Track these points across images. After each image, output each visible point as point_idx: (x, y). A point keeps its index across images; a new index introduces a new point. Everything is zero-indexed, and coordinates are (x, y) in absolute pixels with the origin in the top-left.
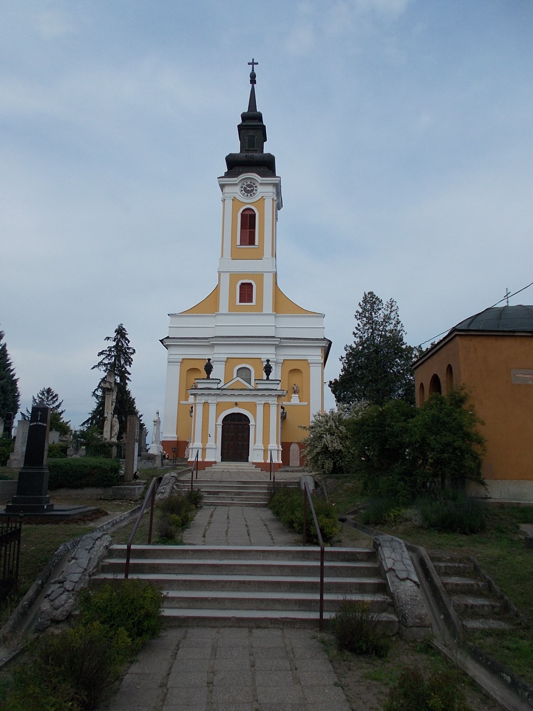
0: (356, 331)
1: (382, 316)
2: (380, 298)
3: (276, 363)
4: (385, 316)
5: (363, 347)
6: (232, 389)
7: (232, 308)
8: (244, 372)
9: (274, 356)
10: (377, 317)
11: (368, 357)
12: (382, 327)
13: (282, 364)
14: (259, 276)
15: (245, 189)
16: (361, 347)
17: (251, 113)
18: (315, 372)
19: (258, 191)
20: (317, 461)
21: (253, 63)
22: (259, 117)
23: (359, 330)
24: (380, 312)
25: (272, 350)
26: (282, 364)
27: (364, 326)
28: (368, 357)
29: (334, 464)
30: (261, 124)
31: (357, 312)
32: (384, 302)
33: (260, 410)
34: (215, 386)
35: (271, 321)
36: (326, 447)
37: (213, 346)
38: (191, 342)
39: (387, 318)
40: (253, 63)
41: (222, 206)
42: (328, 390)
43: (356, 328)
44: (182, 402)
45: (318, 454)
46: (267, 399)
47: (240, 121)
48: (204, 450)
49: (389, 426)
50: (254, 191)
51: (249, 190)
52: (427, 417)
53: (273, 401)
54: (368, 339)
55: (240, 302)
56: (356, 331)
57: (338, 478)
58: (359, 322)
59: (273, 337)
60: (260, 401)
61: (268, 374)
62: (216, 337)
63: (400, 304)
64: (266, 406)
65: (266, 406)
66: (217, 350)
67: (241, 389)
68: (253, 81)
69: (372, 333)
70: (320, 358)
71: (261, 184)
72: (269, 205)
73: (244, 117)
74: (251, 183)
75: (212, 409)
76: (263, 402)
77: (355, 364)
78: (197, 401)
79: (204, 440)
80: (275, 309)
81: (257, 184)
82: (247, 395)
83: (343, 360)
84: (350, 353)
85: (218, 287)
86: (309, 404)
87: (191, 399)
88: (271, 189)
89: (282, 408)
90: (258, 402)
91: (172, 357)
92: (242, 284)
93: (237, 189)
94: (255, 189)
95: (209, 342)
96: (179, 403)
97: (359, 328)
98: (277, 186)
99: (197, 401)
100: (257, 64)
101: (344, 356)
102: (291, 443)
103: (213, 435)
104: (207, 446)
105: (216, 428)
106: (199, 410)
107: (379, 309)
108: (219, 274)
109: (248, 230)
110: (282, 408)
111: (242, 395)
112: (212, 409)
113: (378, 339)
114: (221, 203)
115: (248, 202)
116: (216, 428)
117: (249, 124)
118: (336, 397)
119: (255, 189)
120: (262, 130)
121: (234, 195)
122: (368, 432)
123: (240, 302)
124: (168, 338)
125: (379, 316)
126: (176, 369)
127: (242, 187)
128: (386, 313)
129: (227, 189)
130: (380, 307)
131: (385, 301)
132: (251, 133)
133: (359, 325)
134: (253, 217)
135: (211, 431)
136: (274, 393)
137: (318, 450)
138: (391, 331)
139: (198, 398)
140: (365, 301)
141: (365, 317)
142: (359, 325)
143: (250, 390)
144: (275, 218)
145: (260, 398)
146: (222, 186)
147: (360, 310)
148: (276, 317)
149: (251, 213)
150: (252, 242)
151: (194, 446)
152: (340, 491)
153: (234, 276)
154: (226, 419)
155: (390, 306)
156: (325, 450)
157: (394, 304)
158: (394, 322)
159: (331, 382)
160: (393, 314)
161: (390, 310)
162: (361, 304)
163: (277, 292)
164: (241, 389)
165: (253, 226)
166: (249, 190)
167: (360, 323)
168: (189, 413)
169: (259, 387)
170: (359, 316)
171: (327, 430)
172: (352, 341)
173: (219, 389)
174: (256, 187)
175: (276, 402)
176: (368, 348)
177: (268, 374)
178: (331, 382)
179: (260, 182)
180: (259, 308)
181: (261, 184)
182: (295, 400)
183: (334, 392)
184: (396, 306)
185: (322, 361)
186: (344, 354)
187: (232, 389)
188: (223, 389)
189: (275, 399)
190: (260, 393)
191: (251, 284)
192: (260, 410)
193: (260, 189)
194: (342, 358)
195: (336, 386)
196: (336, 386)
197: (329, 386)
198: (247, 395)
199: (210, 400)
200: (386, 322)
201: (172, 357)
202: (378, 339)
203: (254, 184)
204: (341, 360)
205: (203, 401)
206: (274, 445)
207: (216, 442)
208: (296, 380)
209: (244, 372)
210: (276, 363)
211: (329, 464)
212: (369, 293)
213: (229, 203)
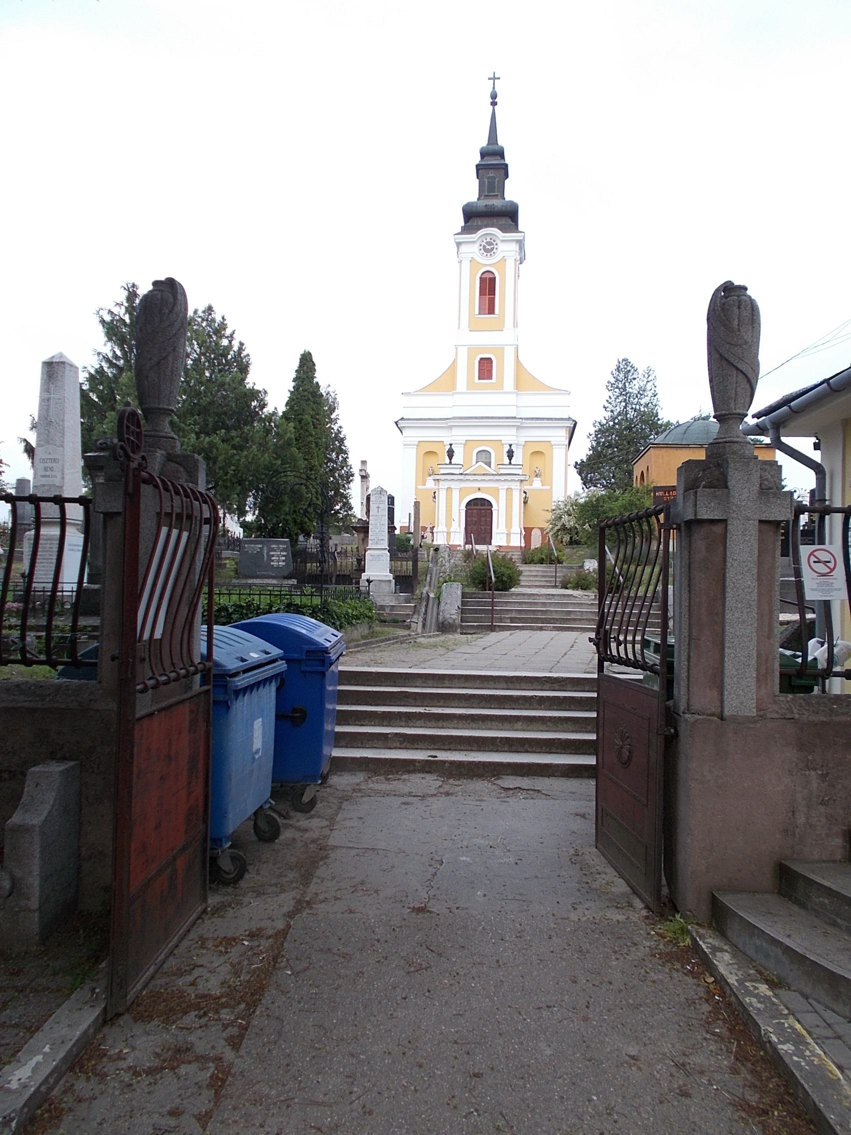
0: (607, 405)
1: (637, 387)
2: (636, 366)
3: (517, 445)
4: (640, 388)
5: (614, 423)
6: (475, 475)
7: (470, 385)
8: (484, 456)
9: (515, 438)
10: (631, 388)
11: (620, 434)
12: (636, 400)
13: (524, 446)
14: (500, 350)
15: (484, 246)
16: (611, 423)
17: (491, 147)
18: (558, 454)
19: (499, 249)
20: (557, 536)
21: (494, 78)
22: (501, 154)
23: (610, 403)
24: (635, 382)
25: (513, 431)
26: (524, 446)
27: (616, 399)
28: (620, 434)
29: (571, 538)
30: (502, 162)
31: (609, 382)
32: (640, 371)
33: (503, 495)
34: (457, 471)
35: (512, 399)
36: (564, 525)
37: (451, 427)
38: (421, 423)
39: (642, 391)
40: (494, 78)
41: (459, 266)
42: (573, 472)
43: (607, 401)
44: (419, 487)
45: (558, 530)
46: (509, 483)
47: (477, 159)
48: (448, 533)
49: (602, 507)
50: (495, 250)
51: (489, 248)
52: (743, 504)
53: (516, 486)
54: (619, 414)
55: (479, 379)
56: (607, 405)
57: (573, 548)
58: (610, 394)
59: (515, 418)
60: (503, 486)
61: (510, 459)
62: (454, 418)
63: (658, 372)
64: (509, 490)
65: (509, 490)
66: (455, 431)
67: (484, 474)
68: (494, 104)
69: (625, 407)
70: (564, 439)
71: (503, 241)
72: (510, 265)
73: (484, 154)
74: (491, 239)
75: (456, 495)
76: (506, 487)
77: (604, 443)
78: (440, 487)
79: (449, 523)
80: (517, 385)
81: (498, 241)
82: (490, 480)
83: (591, 437)
84: (600, 430)
85: (455, 362)
86: (551, 488)
87: (430, 484)
88: (514, 247)
89: (525, 492)
90: (501, 487)
91: (405, 439)
92: (481, 359)
93: (475, 248)
94: (495, 247)
95: (447, 423)
96: (416, 487)
97: (610, 401)
98: (521, 243)
99: (440, 487)
100: (499, 78)
101: (593, 432)
102: (533, 528)
103: (457, 520)
104: (452, 529)
105: (460, 513)
106: (442, 496)
107: (634, 379)
108: (457, 348)
109: (487, 297)
110: (525, 492)
111: (484, 480)
112: (456, 495)
113: (631, 414)
114: (458, 265)
115: (487, 263)
116: (460, 513)
117: (489, 163)
118: (582, 479)
119: (495, 247)
120: (504, 169)
121: (471, 255)
122: (588, 511)
123: (479, 379)
124: (402, 419)
125: (633, 388)
126: (413, 452)
127: (481, 245)
128: (642, 384)
129: (463, 248)
130: (635, 376)
131: (641, 368)
132: (491, 174)
133: (610, 397)
134: (493, 281)
135: (455, 515)
136: (516, 478)
137: (558, 527)
138: (647, 405)
139: (441, 483)
140: (618, 369)
141: (617, 387)
142: (610, 397)
143: (493, 475)
144: (517, 276)
145: (503, 483)
146: (459, 244)
147: (613, 381)
148: (517, 394)
149: (491, 276)
150: (491, 311)
151: (439, 530)
152: (575, 557)
153: (472, 350)
154: (469, 504)
155: (647, 376)
156: (564, 528)
157: (651, 372)
158: (650, 394)
159: (576, 463)
160: (650, 384)
161: (646, 380)
162: (614, 372)
163: (519, 365)
164: (484, 474)
165: (492, 292)
166: (489, 248)
167: (612, 396)
168: (432, 499)
169: (502, 471)
170: (611, 386)
171: (565, 512)
172: (602, 416)
173: (461, 474)
174: (496, 244)
175: (518, 487)
176: (619, 423)
177: (510, 459)
178: (576, 463)
179: (501, 239)
180: (500, 385)
181: (503, 241)
182: (537, 484)
183: (580, 474)
184: (654, 375)
185: (567, 443)
186: (592, 430)
187: (475, 475)
188: (466, 474)
189: (518, 483)
190: (503, 478)
191: (490, 359)
192: (503, 495)
193: (502, 247)
194: (590, 435)
195: (582, 468)
196: (582, 468)
197: (575, 467)
198: (490, 480)
199: (453, 485)
200: (641, 395)
201: (405, 439)
202: (631, 414)
203: (494, 241)
204: (588, 437)
205: (446, 487)
206: (517, 528)
207: (459, 526)
208: (538, 462)
209: (484, 456)
210: (517, 445)
211: (567, 538)
212: (623, 360)
213: (466, 265)
